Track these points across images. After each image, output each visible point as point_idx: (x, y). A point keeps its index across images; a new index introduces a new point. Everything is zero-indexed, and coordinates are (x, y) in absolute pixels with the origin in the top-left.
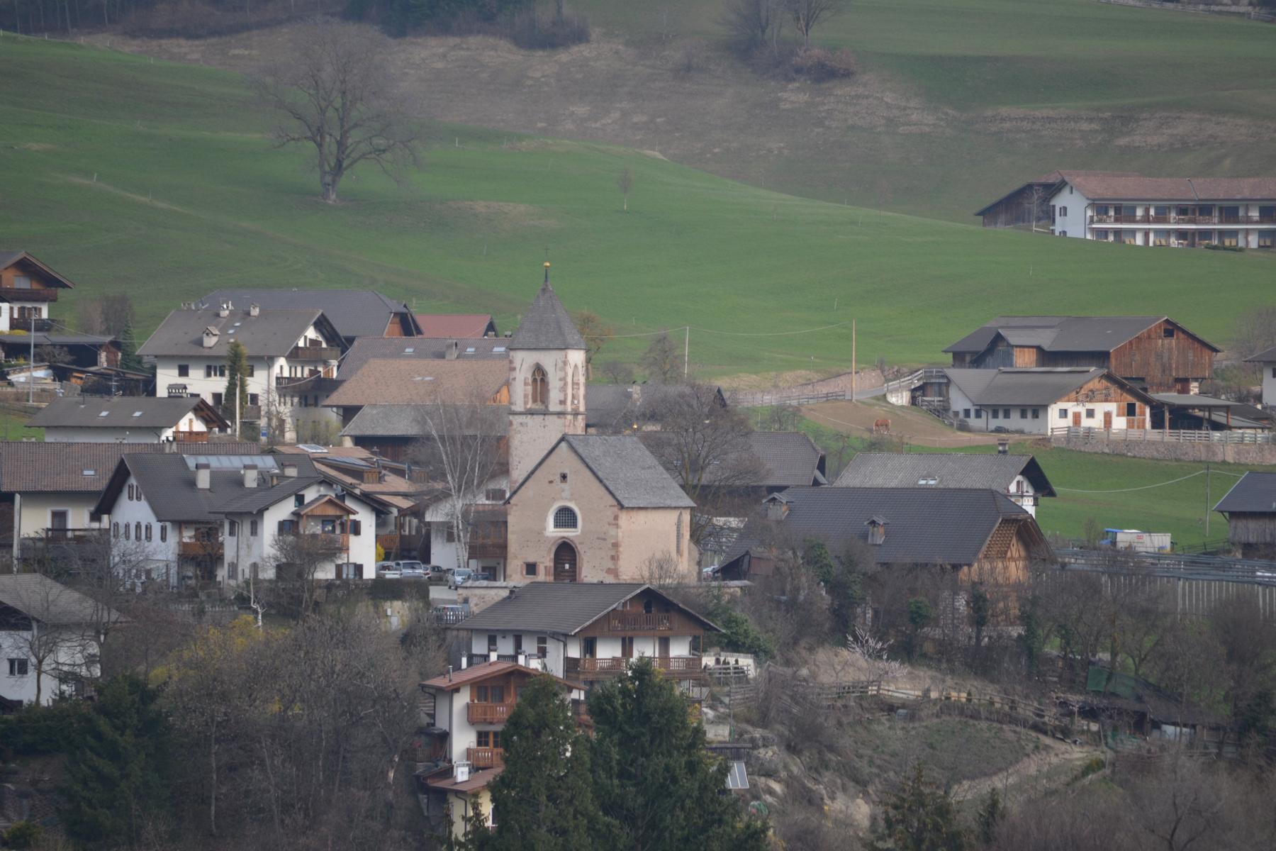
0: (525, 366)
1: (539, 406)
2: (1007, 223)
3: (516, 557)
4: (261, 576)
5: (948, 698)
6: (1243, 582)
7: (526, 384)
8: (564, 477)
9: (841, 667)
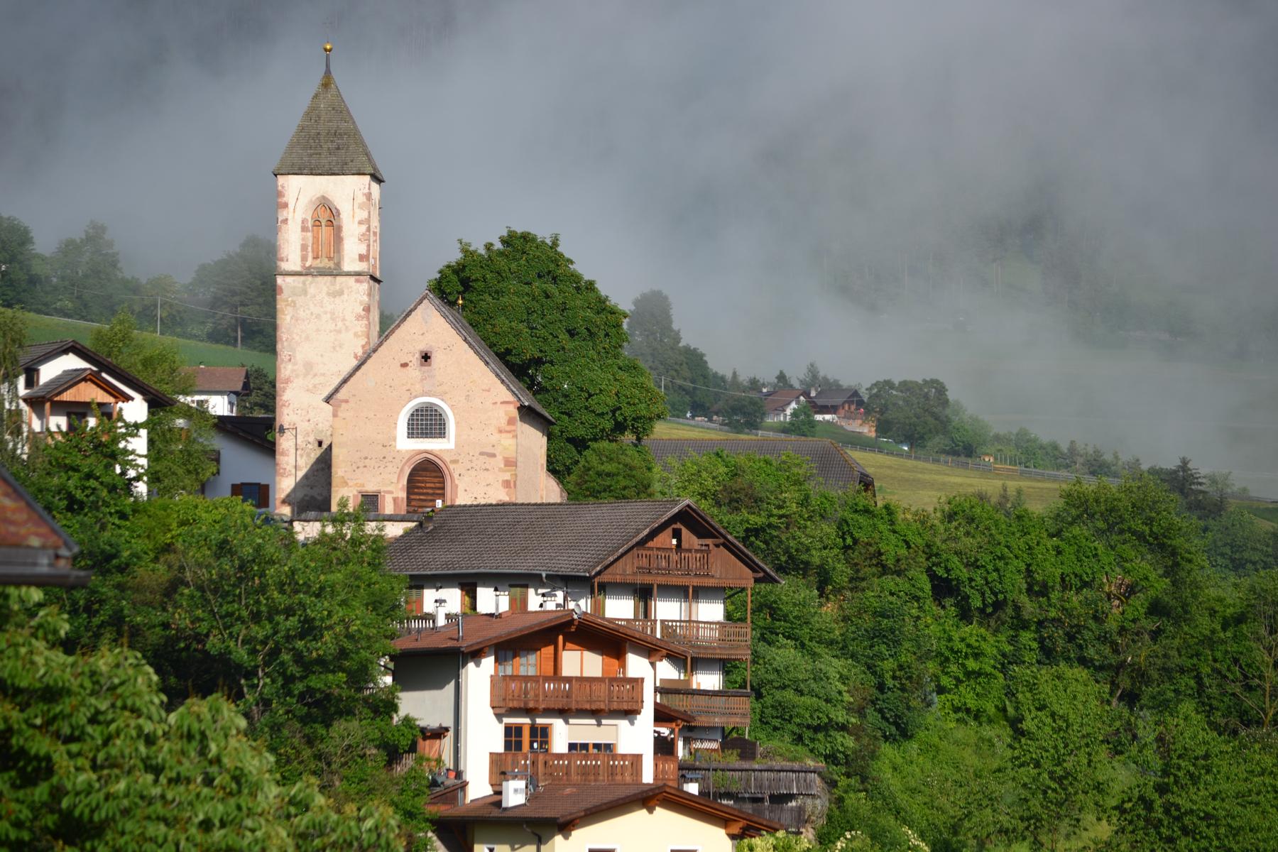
1: (324, 263)
4: (403, 512)
5: (201, 638)
7: (304, 229)
8: (426, 357)
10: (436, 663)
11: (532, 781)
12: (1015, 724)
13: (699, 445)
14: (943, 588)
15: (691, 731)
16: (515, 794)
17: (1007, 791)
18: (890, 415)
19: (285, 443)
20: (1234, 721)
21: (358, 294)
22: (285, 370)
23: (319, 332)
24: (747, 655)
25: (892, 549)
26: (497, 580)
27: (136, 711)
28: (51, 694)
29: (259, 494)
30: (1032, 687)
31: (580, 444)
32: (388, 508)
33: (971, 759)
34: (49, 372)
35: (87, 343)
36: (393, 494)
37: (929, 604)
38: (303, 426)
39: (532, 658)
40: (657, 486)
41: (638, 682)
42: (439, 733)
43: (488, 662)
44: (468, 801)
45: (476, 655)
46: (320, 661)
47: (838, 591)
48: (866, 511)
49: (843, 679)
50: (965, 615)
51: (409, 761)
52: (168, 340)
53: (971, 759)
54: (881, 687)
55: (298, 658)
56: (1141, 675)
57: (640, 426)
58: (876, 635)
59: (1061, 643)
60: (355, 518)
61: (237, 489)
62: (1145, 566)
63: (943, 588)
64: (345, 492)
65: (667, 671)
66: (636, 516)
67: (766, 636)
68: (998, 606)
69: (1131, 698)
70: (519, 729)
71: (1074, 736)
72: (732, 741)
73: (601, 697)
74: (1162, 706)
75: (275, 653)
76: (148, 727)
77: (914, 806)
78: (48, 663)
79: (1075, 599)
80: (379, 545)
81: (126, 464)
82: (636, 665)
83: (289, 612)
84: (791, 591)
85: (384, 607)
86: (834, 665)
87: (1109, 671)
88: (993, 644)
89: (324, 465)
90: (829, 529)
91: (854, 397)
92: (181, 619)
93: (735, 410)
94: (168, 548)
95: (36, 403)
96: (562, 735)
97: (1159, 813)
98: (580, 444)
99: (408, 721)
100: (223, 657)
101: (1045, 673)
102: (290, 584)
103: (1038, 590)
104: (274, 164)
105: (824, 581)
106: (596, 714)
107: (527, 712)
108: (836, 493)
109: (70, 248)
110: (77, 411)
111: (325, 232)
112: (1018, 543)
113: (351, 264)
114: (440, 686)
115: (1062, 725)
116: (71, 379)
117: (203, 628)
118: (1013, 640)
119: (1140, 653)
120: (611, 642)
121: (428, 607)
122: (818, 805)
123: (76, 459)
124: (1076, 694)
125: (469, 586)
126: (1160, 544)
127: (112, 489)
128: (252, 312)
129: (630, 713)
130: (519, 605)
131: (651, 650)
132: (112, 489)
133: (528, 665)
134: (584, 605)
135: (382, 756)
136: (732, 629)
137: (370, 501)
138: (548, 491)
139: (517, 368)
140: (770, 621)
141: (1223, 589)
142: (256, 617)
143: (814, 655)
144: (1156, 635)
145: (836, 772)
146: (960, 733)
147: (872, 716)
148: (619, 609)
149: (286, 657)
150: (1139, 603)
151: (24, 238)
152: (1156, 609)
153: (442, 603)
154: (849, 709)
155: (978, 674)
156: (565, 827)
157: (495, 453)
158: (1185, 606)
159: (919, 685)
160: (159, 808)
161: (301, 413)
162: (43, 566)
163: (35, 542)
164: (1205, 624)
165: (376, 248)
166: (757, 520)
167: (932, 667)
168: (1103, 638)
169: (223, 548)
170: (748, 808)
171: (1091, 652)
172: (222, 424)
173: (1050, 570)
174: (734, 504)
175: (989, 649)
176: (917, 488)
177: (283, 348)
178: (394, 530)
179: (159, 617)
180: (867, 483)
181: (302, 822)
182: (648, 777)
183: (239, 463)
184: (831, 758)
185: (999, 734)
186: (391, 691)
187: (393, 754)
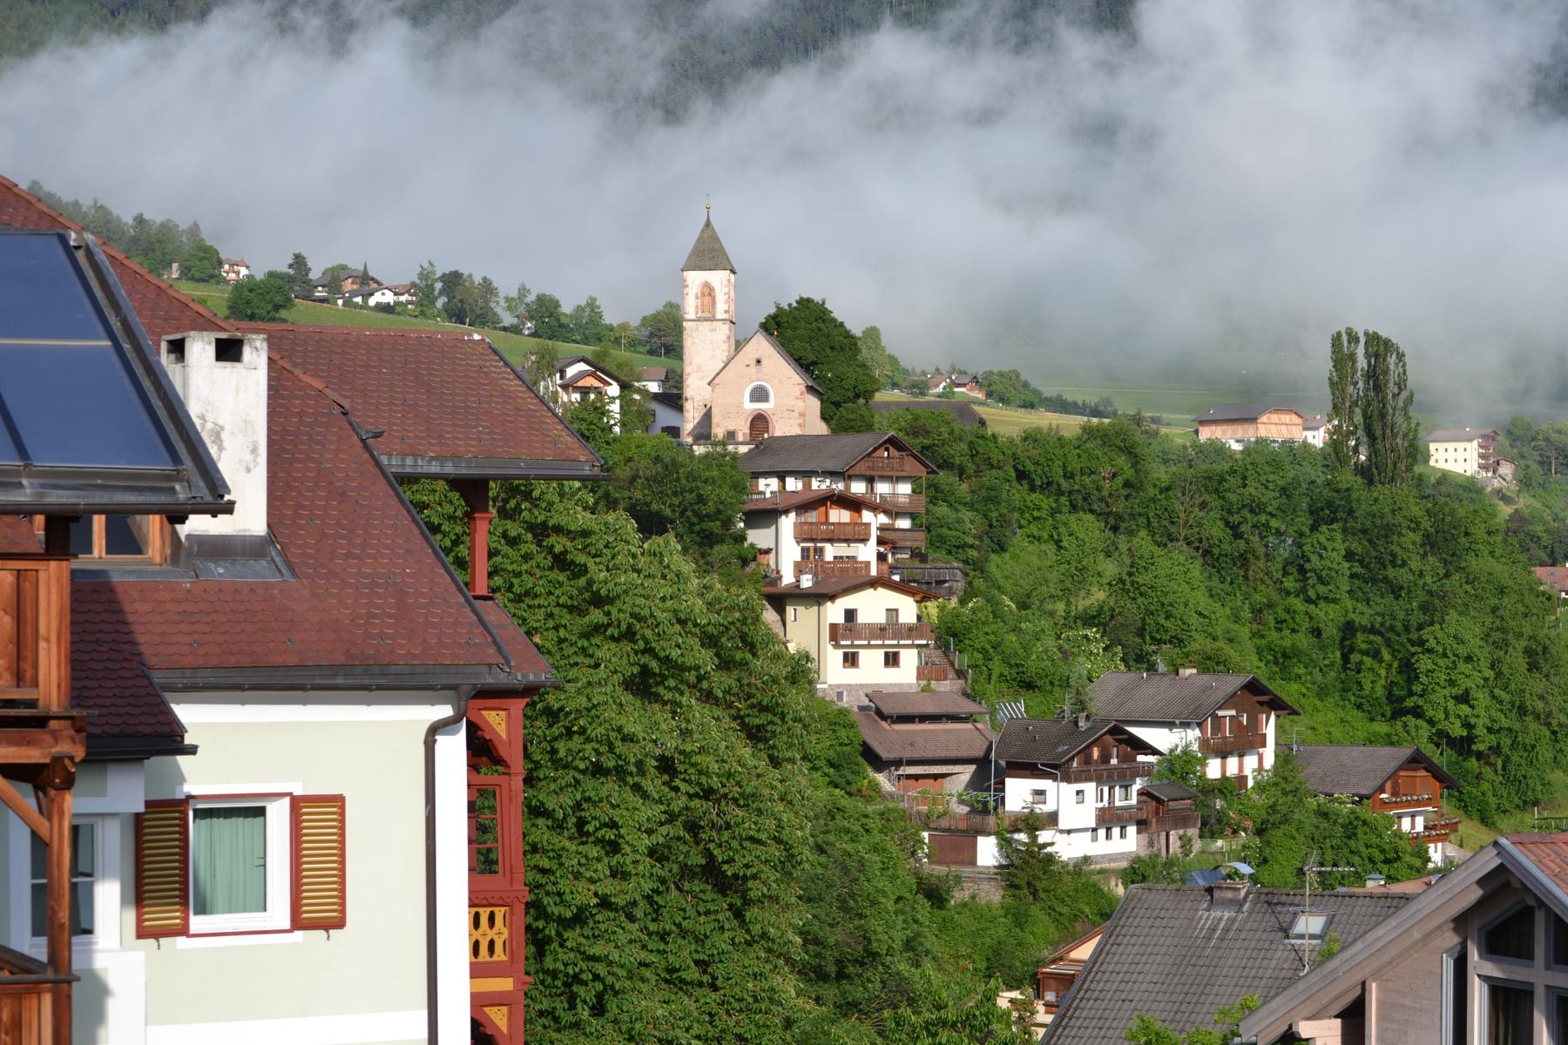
1: (707, 315)
5: (648, 504)
8: (759, 361)
10: (766, 516)
11: (815, 575)
12: (1058, 543)
13: (898, 404)
14: (1022, 475)
15: (895, 549)
16: (807, 582)
17: (1053, 576)
18: (994, 388)
19: (688, 406)
20: (1165, 540)
21: (724, 330)
22: (688, 369)
23: (704, 350)
24: (923, 511)
25: (996, 456)
26: (796, 474)
27: (627, 542)
28: (585, 533)
29: (674, 431)
30: (1065, 525)
31: (837, 405)
32: (741, 439)
33: (1036, 561)
34: (571, 371)
35: (589, 357)
36: (743, 431)
37: (1014, 483)
38: (697, 398)
39: (815, 513)
40: (876, 426)
41: (868, 525)
42: (768, 551)
43: (792, 515)
44: (174, 707)
45: (786, 512)
46: (708, 515)
47: (969, 477)
48: (983, 437)
49: (972, 522)
50: (1033, 489)
51: (753, 565)
52: (628, 354)
53: (1036, 561)
54: (991, 526)
55: (696, 513)
56: (1119, 517)
57: (868, 395)
58: (988, 499)
59: (1080, 502)
60: (724, 444)
61: (664, 429)
62: (1122, 461)
63: (1022, 475)
64: (719, 431)
65: (883, 519)
66: (866, 441)
67: (933, 501)
68: (1049, 484)
69: (1115, 529)
70: (808, 549)
71: (1087, 549)
72: (916, 554)
73: (849, 531)
74: (1131, 533)
75: (685, 510)
76: (634, 550)
77: (1008, 586)
78: (583, 519)
79: (1087, 480)
80: (735, 456)
81: (610, 417)
82: (867, 516)
83: (691, 491)
84: (945, 478)
85: (739, 488)
86: (967, 515)
87: (1103, 515)
88: (1045, 502)
89: (708, 416)
90: (964, 446)
91: (975, 379)
92: (638, 495)
93: (914, 386)
94: (630, 459)
95: (565, 387)
96: (830, 552)
97: (1128, 586)
98: (837, 405)
99: (752, 546)
100: (658, 514)
101: (1073, 518)
102: (691, 477)
103: (1069, 476)
104: (682, 265)
105: (962, 473)
106: (847, 541)
107: (812, 540)
108: (968, 428)
109: (579, 309)
110: (585, 391)
111: (707, 299)
112: (1059, 452)
113: (720, 314)
114: (769, 527)
115: (1081, 544)
116: (582, 375)
117: (648, 499)
118: (1056, 501)
119: (1119, 507)
120: (855, 505)
121: (762, 487)
122: (960, 585)
123: (585, 415)
124: (1088, 527)
125: (782, 477)
126: (1130, 452)
127: (603, 430)
128: (669, 340)
129: (864, 540)
130: (807, 486)
131: (875, 509)
132: (603, 430)
133: (812, 517)
134: (840, 486)
135: (739, 563)
136: (916, 497)
137: (731, 435)
138: (821, 428)
139: (804, 365)
140: (934, 493)
141: (1161, 474)
142: (675, 494)
143: (957, 510)
144: (1127, 497)
145: (968, 569)
146: (1031, 548)
147: (987, 541)
148: (858, 488)
149: (689, 513)
150: (1119, 481)
151: (557, 305)
152: (1127, 484)
153: (768, 486)
154: (974, 537)
155: (1038, 519)
156: (832, 597)
157: (794, 409)
158: (1141, 483)
159: (1010, 523)
160: (640, 591)
161: (696, 390)
162: (587, 471)
163: (583, 458)
164: (1151, 492)
165: (733, 307)
166: (927, 442)
167: (1016, 515)
168: (1101, 500)
169: (657, 459)
170: (924, 587)
171: (1095, 507)
172: (656, 397)
173: (1075, 465)
174: (916, 434)
175: (1044, 506)
176: (1007, 422)
177: (686, 358)
178: (743, 449)
179: (626, 494)
180: (982, 423)
181: (710, 596)
182: (874, 572)
183: (665, 416)
184: (966, 562)
185: (1050, 548)
186: (743, 530)
187: (745, 562)
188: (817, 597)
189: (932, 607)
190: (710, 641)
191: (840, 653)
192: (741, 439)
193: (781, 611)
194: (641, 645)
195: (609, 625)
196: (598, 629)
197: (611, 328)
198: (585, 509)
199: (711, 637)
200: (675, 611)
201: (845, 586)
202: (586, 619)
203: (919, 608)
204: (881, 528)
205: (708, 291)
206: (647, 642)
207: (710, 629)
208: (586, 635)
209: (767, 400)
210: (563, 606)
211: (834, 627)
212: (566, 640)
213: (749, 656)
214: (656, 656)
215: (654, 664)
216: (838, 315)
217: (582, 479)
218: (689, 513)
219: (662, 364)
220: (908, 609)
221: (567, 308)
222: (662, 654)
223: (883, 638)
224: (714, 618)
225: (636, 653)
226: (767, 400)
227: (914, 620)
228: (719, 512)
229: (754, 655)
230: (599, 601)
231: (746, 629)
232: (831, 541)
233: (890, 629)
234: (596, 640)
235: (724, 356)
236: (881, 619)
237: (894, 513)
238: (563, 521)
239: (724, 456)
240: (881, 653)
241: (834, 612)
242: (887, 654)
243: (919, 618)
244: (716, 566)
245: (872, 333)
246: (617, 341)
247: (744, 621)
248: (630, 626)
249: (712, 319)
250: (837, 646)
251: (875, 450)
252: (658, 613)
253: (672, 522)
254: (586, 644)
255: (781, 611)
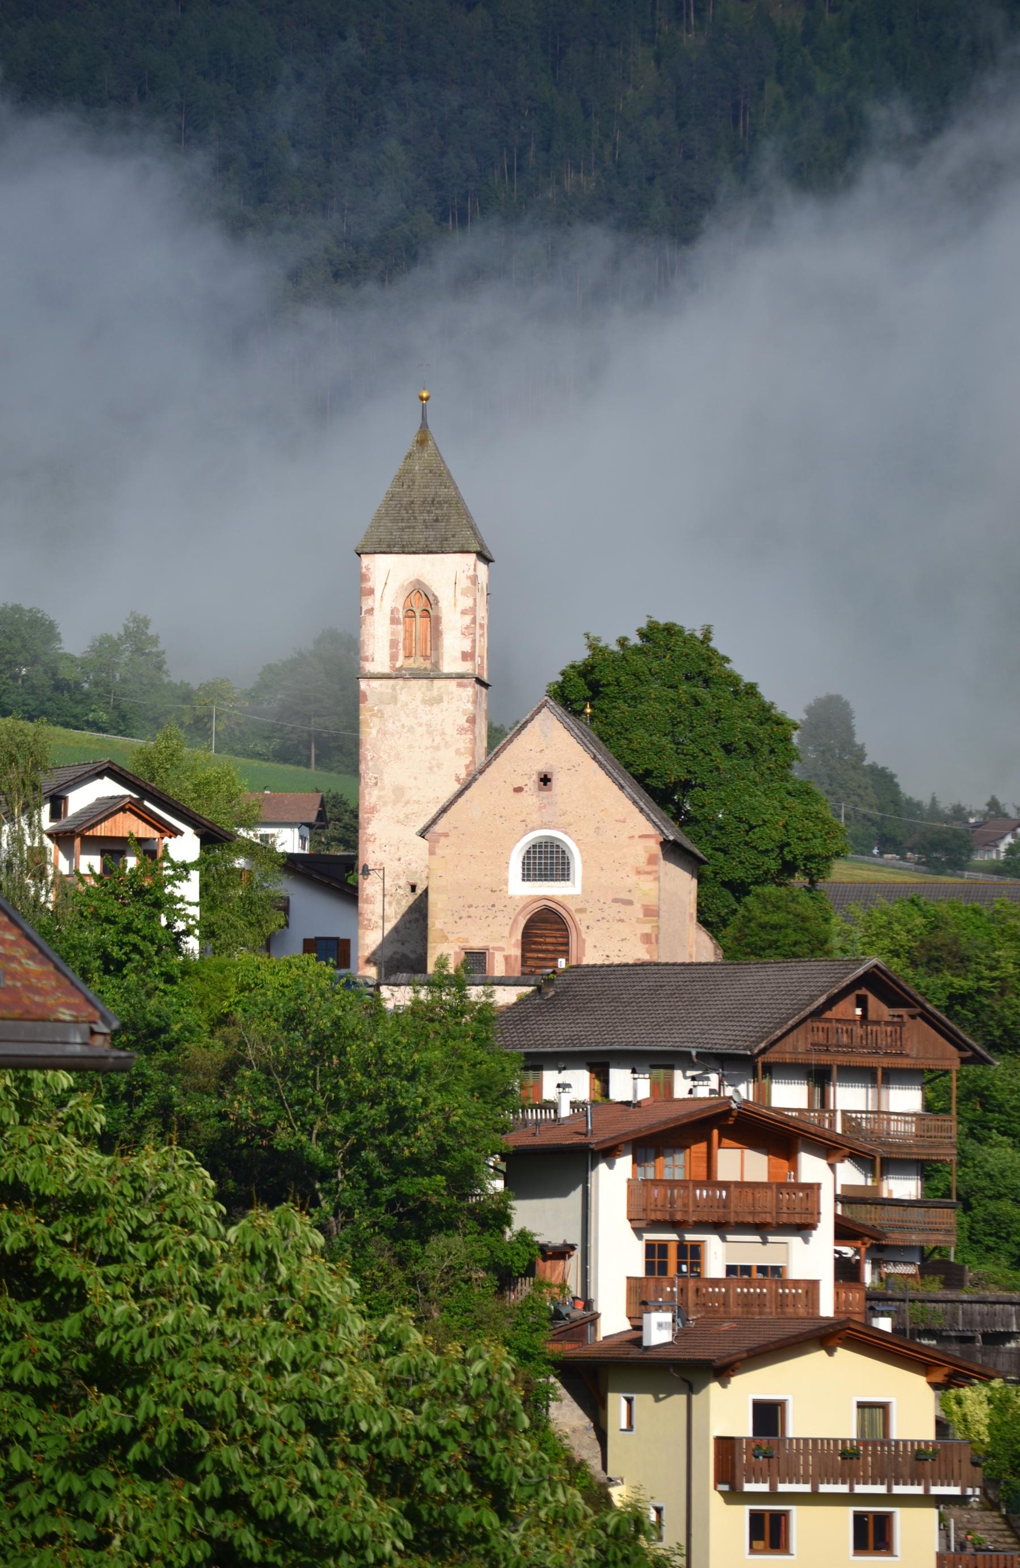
0: (394, 586)
1: (418, 663)
2: (60, 641)
3: (445, 938)
5: (266, 1132)
6: (970, 1302)
7: (394, 621)
8: (545, 780)
9: (408, 1411)
10: (559, 1164)
11: (681, 1314)
13: (890, 891)
15: (881, 1252)
16: (659, 1329)
19: (370, 888)
21: (462, 700)
22: (370, 796)
23: (413, 750)
24: (950, 1155)
26: (635, 1060)
27: (186, 1224)
28: (83, 1203)
29: (337, 950)
31: (739, 889)
32: (499, 969)
34: (80, 800)
35: (128, 765)
36: (505, 951)
39: (680, 1158)
40: (836, 942)
41: (813, 1189)
42: (562, 1252)
43: (625, 1163)
45: (609, 1154)
46: (415, 1161)
51: (525, 1287)
55: (386, 1157)
57: (814, 867)
60: (459, 983)
61: (310, 945)
64: (444, 949)
66: (808, 980)
70: (663, 1247)
72: (933, 1265)
73: (766, 1206)
76: (203, 1245)
78: (82, 1166)
80: (485, 1015)
82: (811, 1167)
83: (374, 1100)
85: (493, 1092)
89: (417, 915)
92: (241, 1107)
94: (224, 1020)
95: (63, 839)
96: (718, 1255)
98: (739, 889)
99: (523, 1236)
100: (295, 1157)
102: (376, 1064)
104: (357, 542)
110: (113, 849)
111: (420, 624)
114: (564, 1193)
116: (107, 809)
120: (779, 1137)
121: (549, 1092)
123: (114, 908)
125: (599, 1066)
129: (804, 1228)
130: (663, 1090)
131: (829, 1149)
133: (675, 1167)
134: (745, 1091)
135: (491, 1281)
136: (931, 1122)
137: (475, 961)
138: (698, 947)
139: (658, 792)
142: (334, 1105)
148: (789, 1096)
153: (566, 1088)
157: (632, 899)
160: (215, 1346)
161: (390, 850)
162: (76, 1045)
163: (65, 1015)
165: (482, 644)
166: (963, 983)
169: (294, 1019)
170: (955, 1349)
172: (292, 864)
177: (368, 769)
178: (506, 996)
179: (212, 1104)
181: (394, 1364)
182: (827, 1308)
183: (312, 913)
186: (503, 1199)
187: (505, 1278)
188: (684, 1372)
189: (975, 1402)
190: (392, 1478)
191: (742, 1513)
192: (499, 969)
193: (595, 1409)
194: (212, 1485)
195: (136, 1435)
196: (108, 1446)
197: (187, 696)
198: (85, 1141)
199: (397, 1467)
200: (303, 1400)
201: (755, 1340)
202: (78, 1421)
203: (943, 1403)
204: (846, 1198)
205: (422, 605)
206: (227, 1477)
207: (394, 1448)
208: (69, 1463)
209: (564, 874)
210: (22, 1388)
211: (726, 1445)
212: (25, 1475)
213: (490, 1518)
214: (252, 1516)
215: (246, 1537)
216: (744, 666)
217: (70, 1065)
218: (369, 1155)
219: (307, 786)
220: (913, 1407)
221: (74, 642)
222: (267, 1510)
223: (850, 1476)
224: (404, 1418)
225: (199, 1504)
226: (564, 874)
227: (927, 1432)
228: (443, 1151)
229: (504, 1515)
230: (114, 1374)
231: (482, 1447)
232: (720, 1228)
233: (870, 1455)
234: (101, 1476)
235: (459, 766)
236: (846, 1428)
237: (879, 1160)
238: (29, 1171)
239: (458, 1013)
240: (845, 1515)
241: (727, 1408)
242: (859, 1520)
243: (942, 1426)
244: (435, 1287)
245: (832, 717)
246: (199, 727)
247: (479, 1429)
248: (183, 1437)
249: (433, 674)
250: (734, 1496)
251: (832, 1002)
252: (258, 1406)
253: (325, 1175)
254: (78, 1485)
255: (595, 1409)
